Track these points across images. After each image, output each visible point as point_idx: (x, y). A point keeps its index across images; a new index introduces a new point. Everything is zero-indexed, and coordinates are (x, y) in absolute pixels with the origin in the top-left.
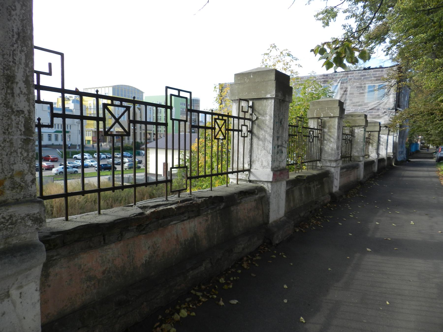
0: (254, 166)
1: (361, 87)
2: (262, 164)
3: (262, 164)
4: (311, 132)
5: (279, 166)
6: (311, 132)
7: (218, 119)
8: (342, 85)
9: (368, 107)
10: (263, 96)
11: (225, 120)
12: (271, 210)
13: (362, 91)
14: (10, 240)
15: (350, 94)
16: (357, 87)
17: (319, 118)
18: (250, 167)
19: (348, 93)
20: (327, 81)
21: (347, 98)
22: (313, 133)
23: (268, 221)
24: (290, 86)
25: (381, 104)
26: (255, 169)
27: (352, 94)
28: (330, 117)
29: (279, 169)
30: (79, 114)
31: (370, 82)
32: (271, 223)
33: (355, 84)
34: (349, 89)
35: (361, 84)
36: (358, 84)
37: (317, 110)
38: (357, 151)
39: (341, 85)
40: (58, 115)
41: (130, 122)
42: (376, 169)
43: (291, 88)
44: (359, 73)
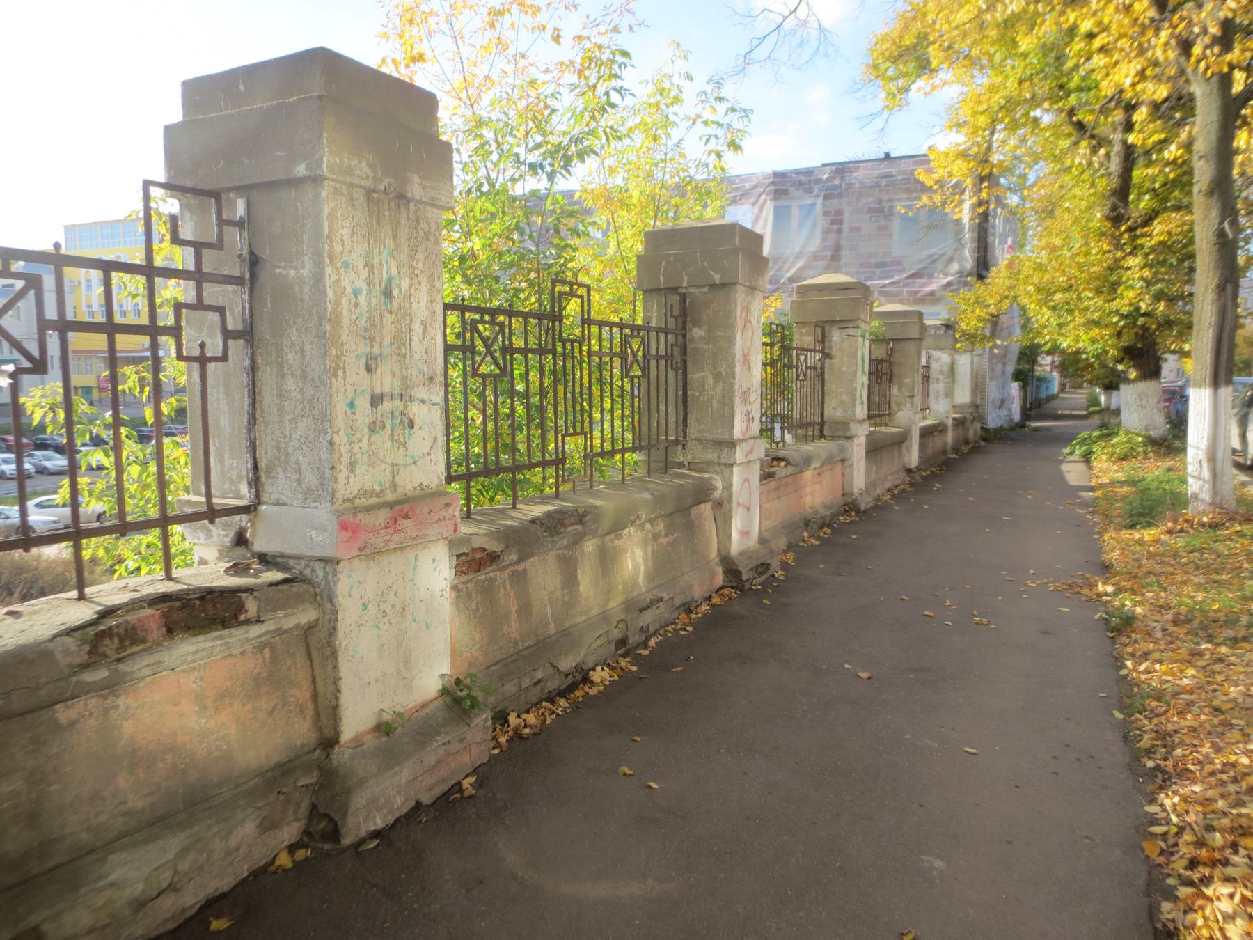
0: (271, 490)
1: (881, 210)
2: (299, 482)
3: (299, 482)
4: (802, 358)
5: (394, 485)
6: (802, 358)
7: (482, 321)
8: (828, 202)
9: (903, 271)
10: (279, 175)
11: (502, 325)
12: (345, 685)
13: (882, 222)
14: (544, 574)
15: (852, 230)
16: (871, 210)
17: (674, 290)
18: (258, 496)
19: (845, 226)
20: (785, 192)
21: (843, 243)
22: (806, 359)
23: (337, 734)
24: (444, 138)
25: (936, 260)
26: (277, 504)
27: (858, 229)
28: (713, 286)
29: (390, 497)
30: (144, 320)
31: (905, 196)
32: (358, 741)
33: (864, 201)
34: (846, 217)
35: (881, 201)
36: (871, 200)
37: (668, 262)
38: (842, 402)
39: (824, 205)
40: (166, 331)
41: (43, 325)
42: (913, 457)
43: (447, 147)
44: (873, 169)
